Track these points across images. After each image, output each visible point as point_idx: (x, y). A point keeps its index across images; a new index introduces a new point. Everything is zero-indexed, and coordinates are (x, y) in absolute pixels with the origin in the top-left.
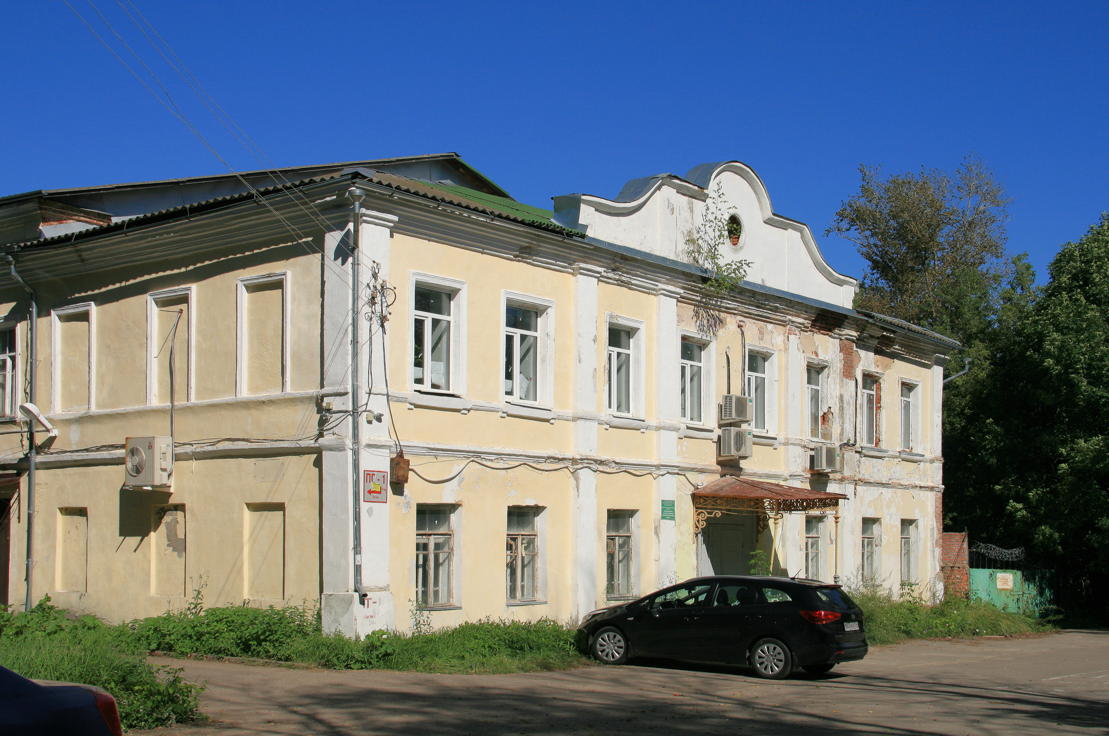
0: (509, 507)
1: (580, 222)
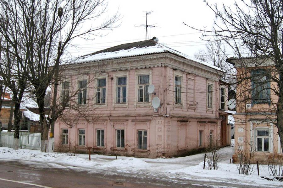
1: (39, 115)
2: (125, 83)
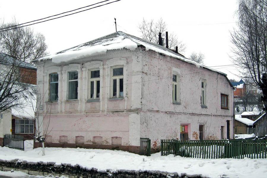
1: (139, 145)
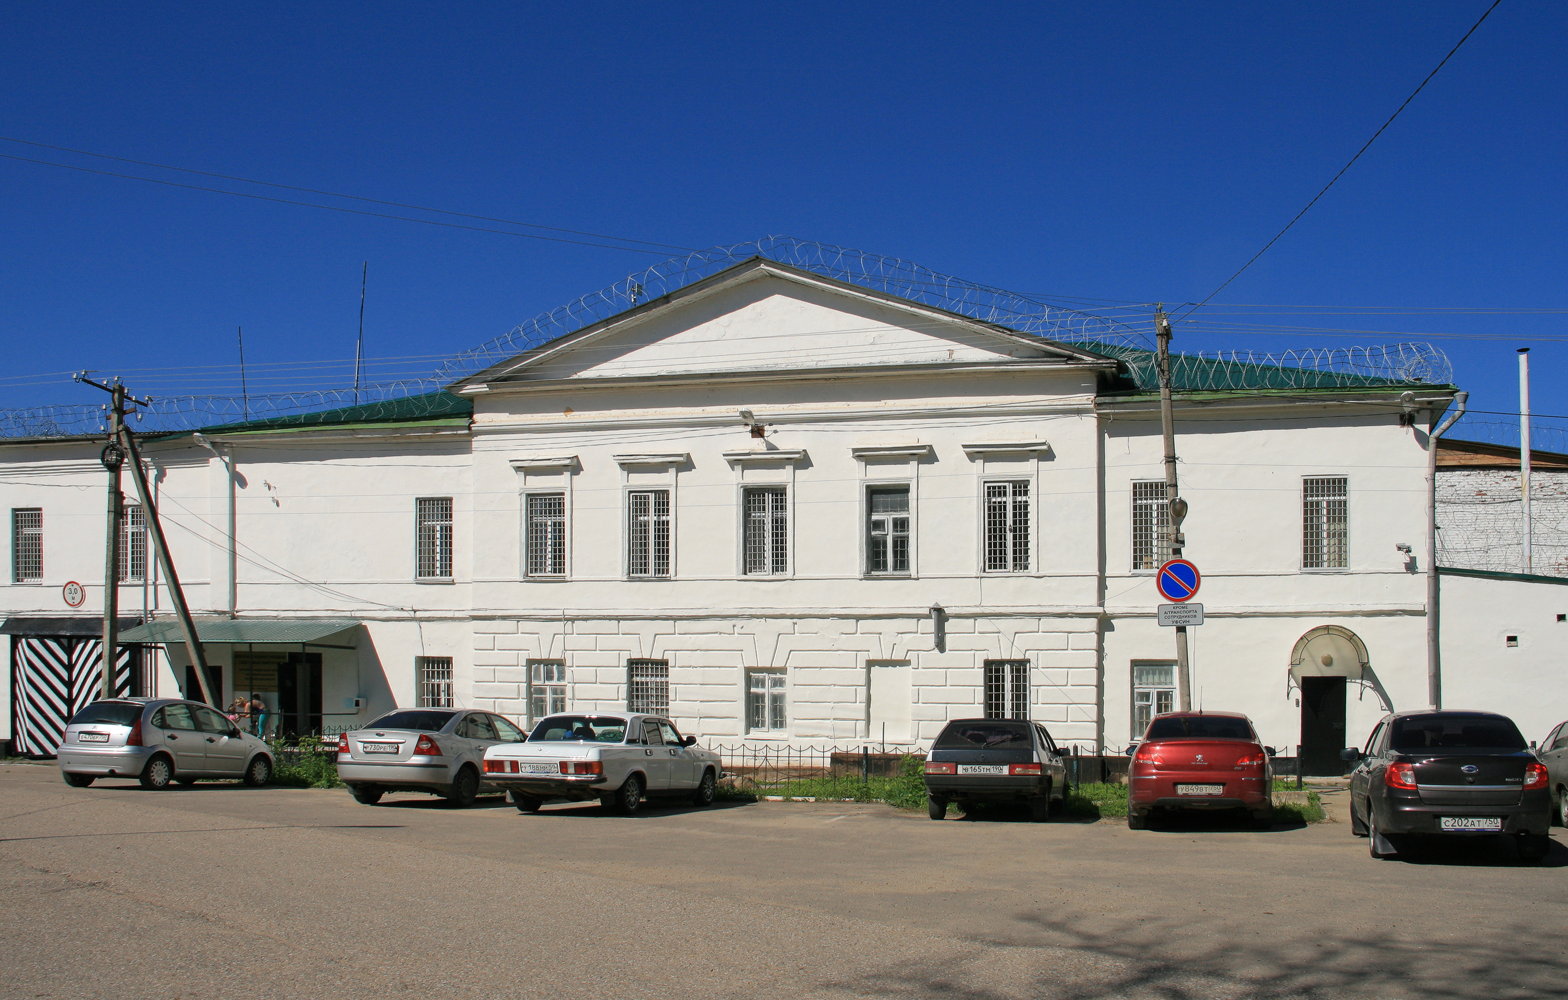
0: (582, 470)
1: (982, 716)
2: (904, 506)
